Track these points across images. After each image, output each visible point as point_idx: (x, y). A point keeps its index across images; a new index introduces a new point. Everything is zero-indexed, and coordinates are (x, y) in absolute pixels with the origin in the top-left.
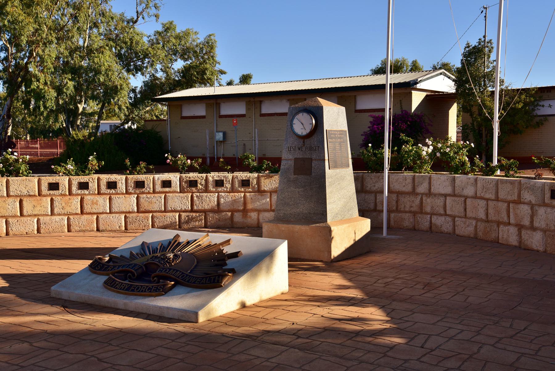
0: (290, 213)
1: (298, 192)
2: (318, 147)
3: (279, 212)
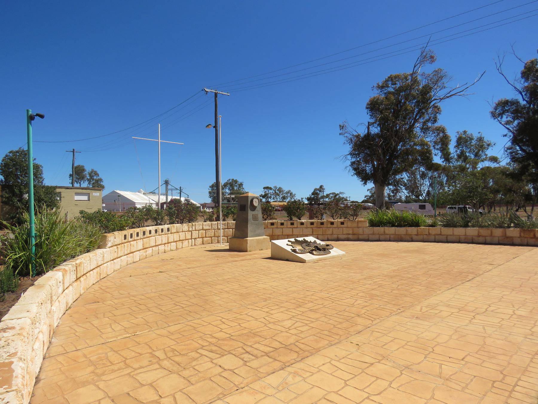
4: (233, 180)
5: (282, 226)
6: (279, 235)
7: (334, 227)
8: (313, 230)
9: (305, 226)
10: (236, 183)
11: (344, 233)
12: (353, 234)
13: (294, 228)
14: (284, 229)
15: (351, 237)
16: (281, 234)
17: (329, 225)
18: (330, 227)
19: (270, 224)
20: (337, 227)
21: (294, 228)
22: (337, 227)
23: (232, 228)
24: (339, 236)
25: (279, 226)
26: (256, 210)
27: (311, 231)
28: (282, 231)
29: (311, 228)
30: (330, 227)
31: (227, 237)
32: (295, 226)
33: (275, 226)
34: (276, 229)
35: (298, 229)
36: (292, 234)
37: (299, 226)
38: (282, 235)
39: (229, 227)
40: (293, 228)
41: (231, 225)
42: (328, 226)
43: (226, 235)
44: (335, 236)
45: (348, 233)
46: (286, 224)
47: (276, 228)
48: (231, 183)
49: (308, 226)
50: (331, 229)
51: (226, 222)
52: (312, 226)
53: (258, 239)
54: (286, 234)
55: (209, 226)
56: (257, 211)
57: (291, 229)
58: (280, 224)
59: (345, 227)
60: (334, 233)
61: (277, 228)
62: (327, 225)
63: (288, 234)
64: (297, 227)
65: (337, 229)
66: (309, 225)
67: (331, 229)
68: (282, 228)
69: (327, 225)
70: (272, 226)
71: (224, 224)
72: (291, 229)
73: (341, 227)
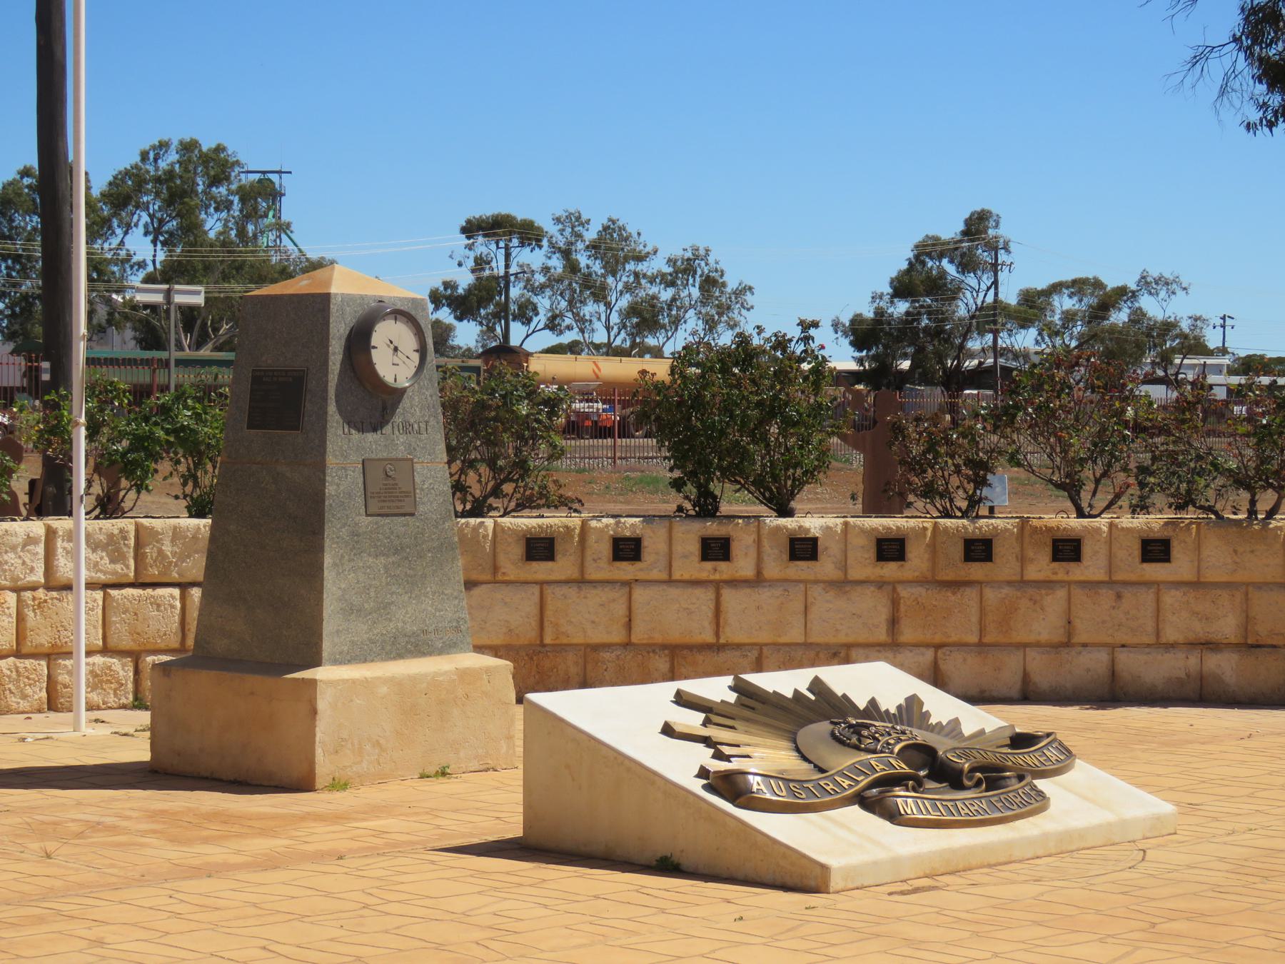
0: (370, 640)
1: (385, 567)
2: (427, 422)
3: (336, 640)
4: (188, 147)
5: (626, 570)
6: (596, 648)
7: (1085, 584)
8: (895, 603)
9: (825, 567)
10: (215, 181)
11: (1170, 635)
12: (1249, 646)
13: (734, 583)
14: (727, 594)
15: (1225, 666)
16: (617, 636)
17: (1041, 566)
18: (1048, 584)
19: (518, 550)
20: (1110, 583)
21: (734, 583)
22: (1110, 583)
23: (175, 576)
24: (1123, 658)
25: (601, 566)
26: (398, 419)
27: (883, 614)
28: (620, 609)
29: (880, 584)
30: (1048, 584)
31: (135, 656)
32: (742, 564)
33: (562, 567)
34: (571, 591)
35: (765, 596)
36: (709, 637)
37: (776, 565)
38: (627, 645)
39: (153, 572)
40: (717, 585)
41: (167, 548)
42: (1033, 573)
43: (127, 643)
44: (1091, 664)
45: (1199, 629)
46: (662, 547)
47: (567, 582)
48: (170, 174)
49: (855, 574)
50: (1061, 593)
51: (127, 524)
52: (890, 570)
53: (414, 679)
54: (658, 638)
55: (117, 556)
56: (407, 428)
57: (704, 598)
58: (606, 549)
59: (1178, 584)
60: (1081, 637)
61: (581, 582)
62: (1023, 560)
63: (675, 635)
64: (758, 580)
65: (1107, 596)
66: (864, 565)
67: (1055, 602)
68: (628, 584)
69: (1023, 560)
70: (541, 570)
71: (112, 546)
72: (704, 598)
73: (1147, 584)
